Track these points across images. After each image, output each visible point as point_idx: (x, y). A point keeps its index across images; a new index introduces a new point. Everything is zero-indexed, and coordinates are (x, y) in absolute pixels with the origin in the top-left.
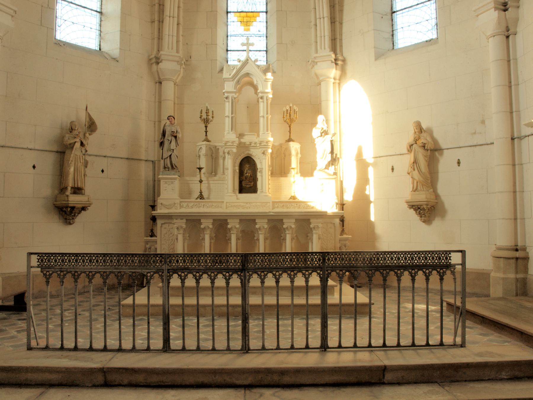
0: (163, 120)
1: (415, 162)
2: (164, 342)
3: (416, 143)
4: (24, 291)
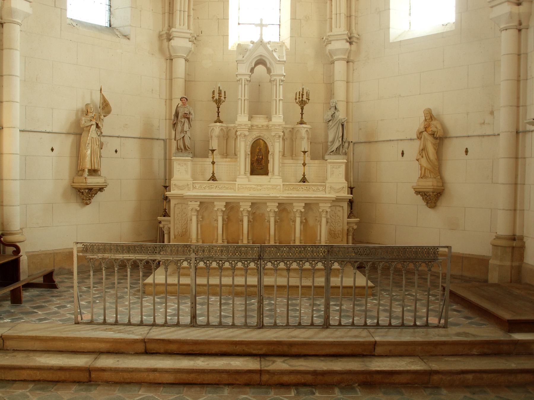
0: (175, 98)
1: (424, 149)
2: (191, 319)
3: (426, 131)
4: (53, 270)
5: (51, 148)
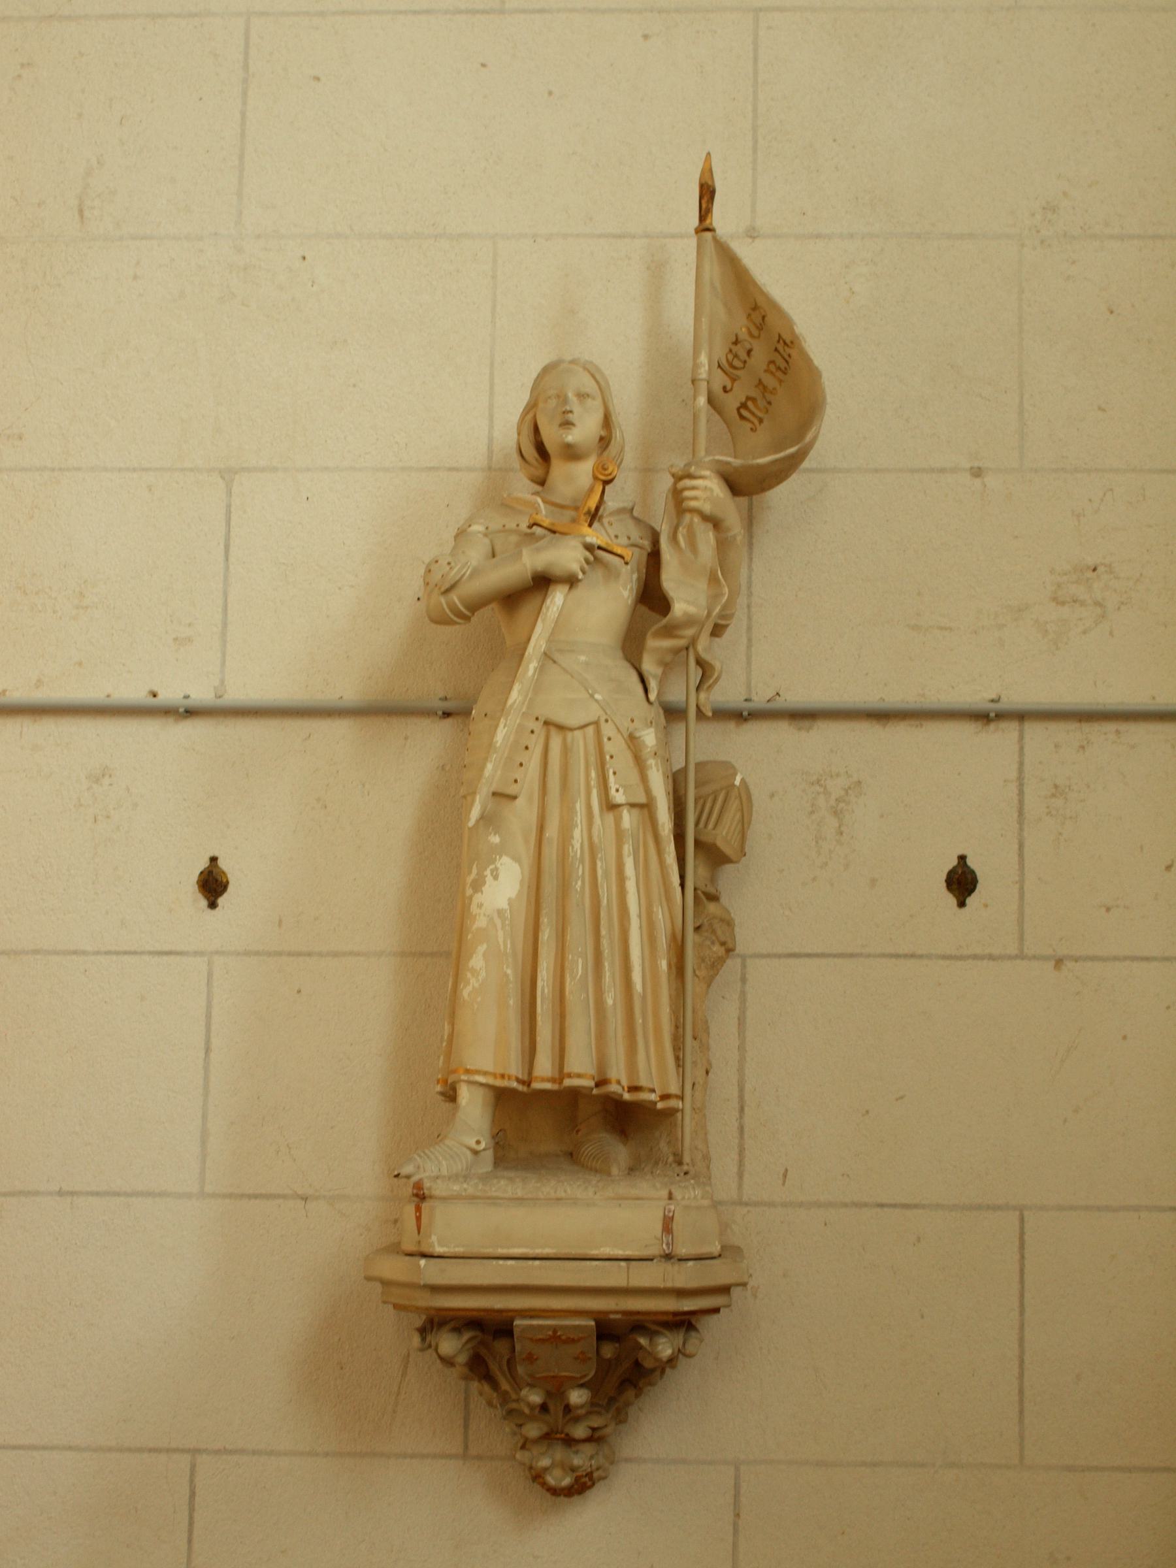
5: (203, 864)
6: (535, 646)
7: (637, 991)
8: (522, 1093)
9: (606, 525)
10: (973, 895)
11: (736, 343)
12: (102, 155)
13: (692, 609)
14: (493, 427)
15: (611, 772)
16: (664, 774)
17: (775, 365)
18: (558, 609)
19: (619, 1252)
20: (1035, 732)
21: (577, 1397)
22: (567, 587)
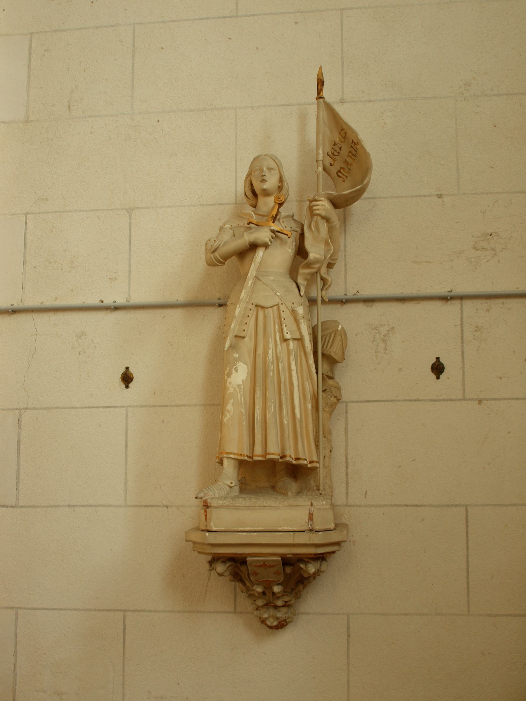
5: (123, 370)
6: (251, 274)
7: (297, 417)
8: (249, 462)
9: (281, 222)
10: (443, 374)
11: (334, 145)
12: (77, 85)
13: (318, 256)
14: (237, 186)
15: (284, 325)
16: (307, 326)
17: (351, 153)
18: (260, 258)
19: (290, 529)
20: (468, 304)
21: (277, 589)
22: (264, 249)
